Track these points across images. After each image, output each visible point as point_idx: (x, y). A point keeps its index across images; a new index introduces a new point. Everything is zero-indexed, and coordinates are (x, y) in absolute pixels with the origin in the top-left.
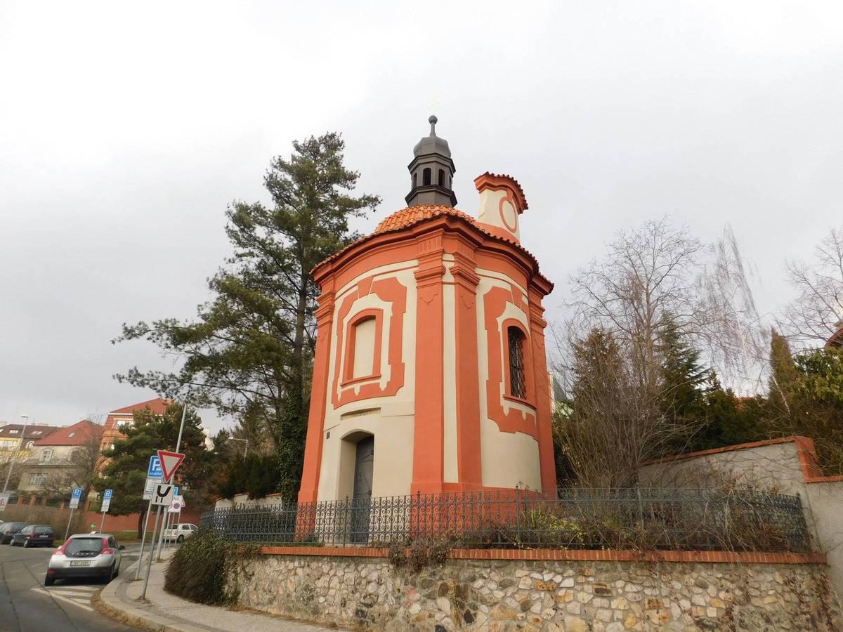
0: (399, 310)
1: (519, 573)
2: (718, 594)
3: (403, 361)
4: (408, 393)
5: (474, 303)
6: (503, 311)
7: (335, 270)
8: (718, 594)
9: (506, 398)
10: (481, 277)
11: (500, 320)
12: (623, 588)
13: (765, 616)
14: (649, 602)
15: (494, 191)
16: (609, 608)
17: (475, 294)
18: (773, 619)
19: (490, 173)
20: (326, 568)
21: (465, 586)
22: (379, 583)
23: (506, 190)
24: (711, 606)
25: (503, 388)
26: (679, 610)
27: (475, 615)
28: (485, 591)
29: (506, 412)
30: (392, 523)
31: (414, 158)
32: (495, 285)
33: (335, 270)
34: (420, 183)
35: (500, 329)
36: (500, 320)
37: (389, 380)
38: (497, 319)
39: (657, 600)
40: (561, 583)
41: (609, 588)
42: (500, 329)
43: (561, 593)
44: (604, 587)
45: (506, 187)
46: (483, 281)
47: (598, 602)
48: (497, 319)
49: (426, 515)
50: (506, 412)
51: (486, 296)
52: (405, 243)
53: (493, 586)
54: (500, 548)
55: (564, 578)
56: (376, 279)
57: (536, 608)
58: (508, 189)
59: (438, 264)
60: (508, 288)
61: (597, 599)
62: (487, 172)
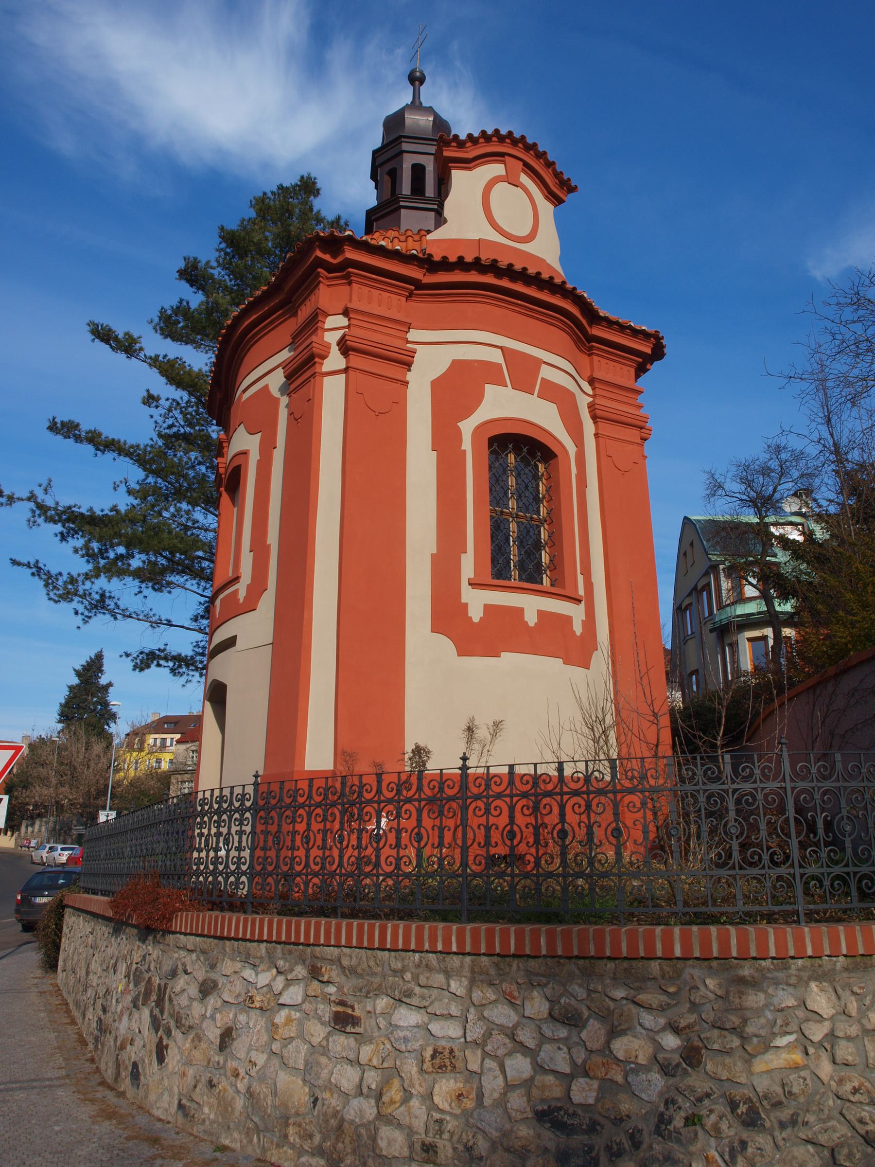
0: (267, 447)
2: (608, 1043)
4: (267, 602)
5: (400, 404)
8: (608, 1043)
9: (473, 584)
12: (387, 1014)
13: (742, 1109)
14: (436, 1053)
15: (470, 169)
16: (355, 1062)
17: (407, 383)
18: (769, 1119)
19: (490, 132)
21: (166, 984)
23: (504, 162)
24: (586, 1074)
26: (500, 1081)
27: (167, 1047)
29: (476, 614)
31: (379, 145)
34: (406, 188)
35: (467, 445)
36: (467, 427)
37: (249, 582)
39: (451, 1051)
41: (357, 1013)
42: (467, 445)
43: (281, 1017)
44: (350, 1011)
45: (502, 155)
46: (422, 355)
47: (341, 1043)
49: (323, 848)
50: (476, 614)
51: (436, 384)
52: (450, 295)
54: (743, 922)
55: (289, 983)
58: (507, 158)
60: (496, 357)
61: (336, 1037)
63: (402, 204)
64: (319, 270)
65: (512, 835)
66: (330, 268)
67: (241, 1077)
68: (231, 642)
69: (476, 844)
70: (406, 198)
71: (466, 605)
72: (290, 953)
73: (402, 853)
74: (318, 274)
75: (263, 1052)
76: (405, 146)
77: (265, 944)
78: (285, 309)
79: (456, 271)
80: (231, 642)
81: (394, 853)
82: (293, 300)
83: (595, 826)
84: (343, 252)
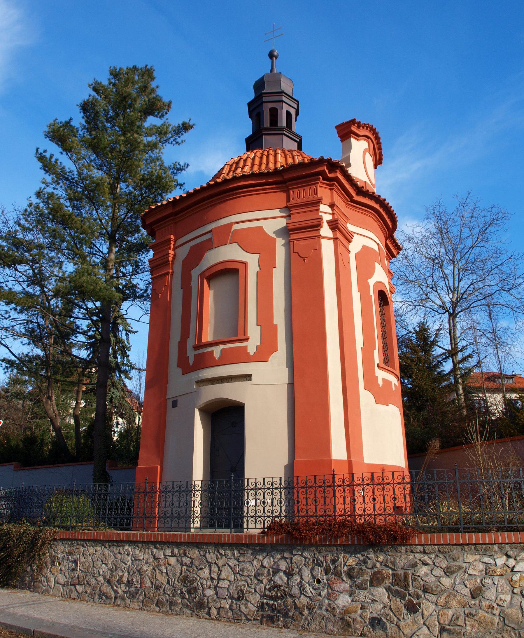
1: (470, 558)
3: (275, 323)
6: (374, 272)
7: (176, 214)
10: (355, 235)
11: (372, 282)
20: (211, 556)
22: (289, 574)
25: (377, 356)
28: (431, 579)
30: (172, 500)
32: (365, 244)
33: (176, 214)
34: (267, 123)
35: (372, 293)
38: (368, 280)
40: (514, 567)
42: (372, 293)
45: (368, 137)
48: (368, 280)
51: (356, 255)
53: (438, 572)
56: (235, 227)
57: (491, 594)
59: (310, 216)
62: (355, 119)
63: (264, 132)
64: (321, 177)
65: (395, 499)
66: (326, 178)
67: (495, 608)
68: (248, 377)
69: (340, 503)
70: (267, 129)
71: (377, 377)
72: (516, 548)
73: (274, 508)
74: (319, 179)
75: (508, 595)
76: (265, 99)
77: (497, 545)
78: (278, 186)
79: (367, 198)
80: (248, 377)
81: (271, 508)
82: (288, 184)
83: (386, 496)
84: (336, 172)
